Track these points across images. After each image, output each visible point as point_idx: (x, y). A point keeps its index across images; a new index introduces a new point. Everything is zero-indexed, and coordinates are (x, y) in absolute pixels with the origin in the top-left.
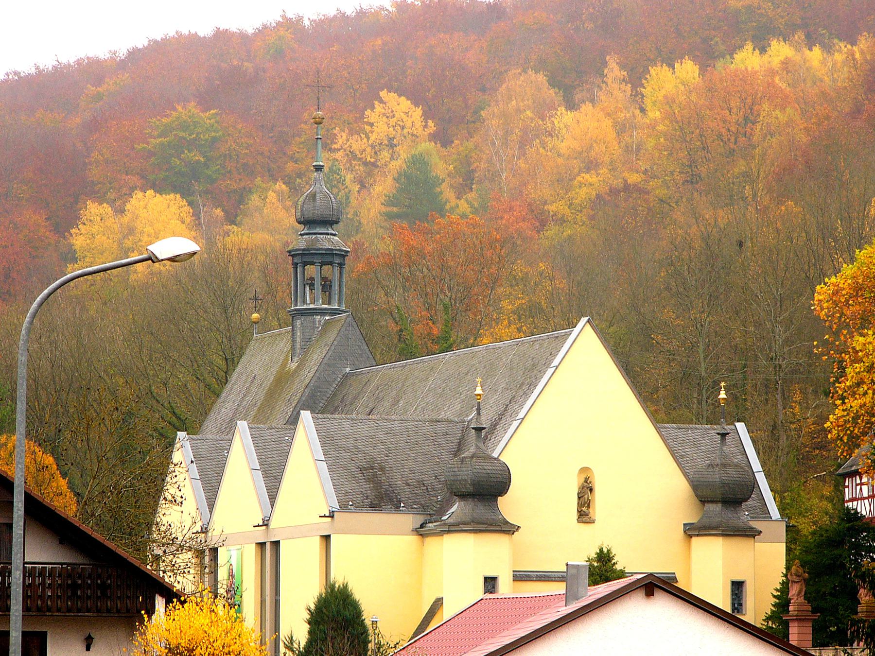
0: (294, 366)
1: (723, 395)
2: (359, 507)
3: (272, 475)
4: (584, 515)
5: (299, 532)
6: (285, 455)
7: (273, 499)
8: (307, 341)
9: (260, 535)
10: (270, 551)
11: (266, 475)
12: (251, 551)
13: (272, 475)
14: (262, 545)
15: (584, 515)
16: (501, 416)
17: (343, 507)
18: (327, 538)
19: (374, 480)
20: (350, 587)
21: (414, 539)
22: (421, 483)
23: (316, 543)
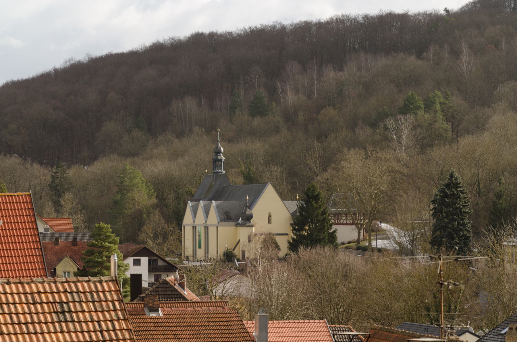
0: (213, 184)
1: (298, 197)
2: (224, 221)
3: (207, 212)
4: (269, 222)
5: (212, 225)
6: (209, 210)
7: (207, 217)
8: (216, 178)
9: (193, 225)
10: (207, 228)
11: (206, 212)
12: (203, 228)
13: (207, 212)
14: (205, 227)
15: (269, 222)
16: (253, 201)
17: (221, 221)
18: (217, 227)
19: (227, 215)
20: (90, 53)
21: (234, 227)
22: (237, 215)
23: (215, 228)
